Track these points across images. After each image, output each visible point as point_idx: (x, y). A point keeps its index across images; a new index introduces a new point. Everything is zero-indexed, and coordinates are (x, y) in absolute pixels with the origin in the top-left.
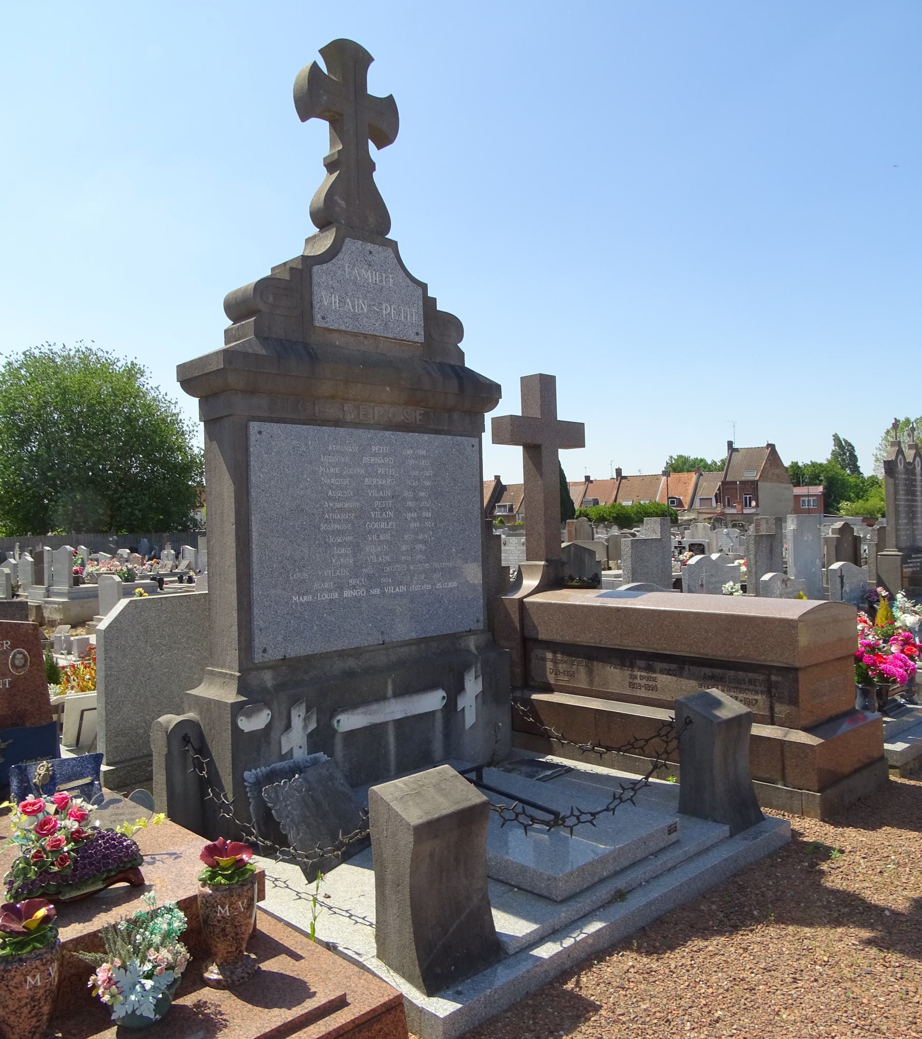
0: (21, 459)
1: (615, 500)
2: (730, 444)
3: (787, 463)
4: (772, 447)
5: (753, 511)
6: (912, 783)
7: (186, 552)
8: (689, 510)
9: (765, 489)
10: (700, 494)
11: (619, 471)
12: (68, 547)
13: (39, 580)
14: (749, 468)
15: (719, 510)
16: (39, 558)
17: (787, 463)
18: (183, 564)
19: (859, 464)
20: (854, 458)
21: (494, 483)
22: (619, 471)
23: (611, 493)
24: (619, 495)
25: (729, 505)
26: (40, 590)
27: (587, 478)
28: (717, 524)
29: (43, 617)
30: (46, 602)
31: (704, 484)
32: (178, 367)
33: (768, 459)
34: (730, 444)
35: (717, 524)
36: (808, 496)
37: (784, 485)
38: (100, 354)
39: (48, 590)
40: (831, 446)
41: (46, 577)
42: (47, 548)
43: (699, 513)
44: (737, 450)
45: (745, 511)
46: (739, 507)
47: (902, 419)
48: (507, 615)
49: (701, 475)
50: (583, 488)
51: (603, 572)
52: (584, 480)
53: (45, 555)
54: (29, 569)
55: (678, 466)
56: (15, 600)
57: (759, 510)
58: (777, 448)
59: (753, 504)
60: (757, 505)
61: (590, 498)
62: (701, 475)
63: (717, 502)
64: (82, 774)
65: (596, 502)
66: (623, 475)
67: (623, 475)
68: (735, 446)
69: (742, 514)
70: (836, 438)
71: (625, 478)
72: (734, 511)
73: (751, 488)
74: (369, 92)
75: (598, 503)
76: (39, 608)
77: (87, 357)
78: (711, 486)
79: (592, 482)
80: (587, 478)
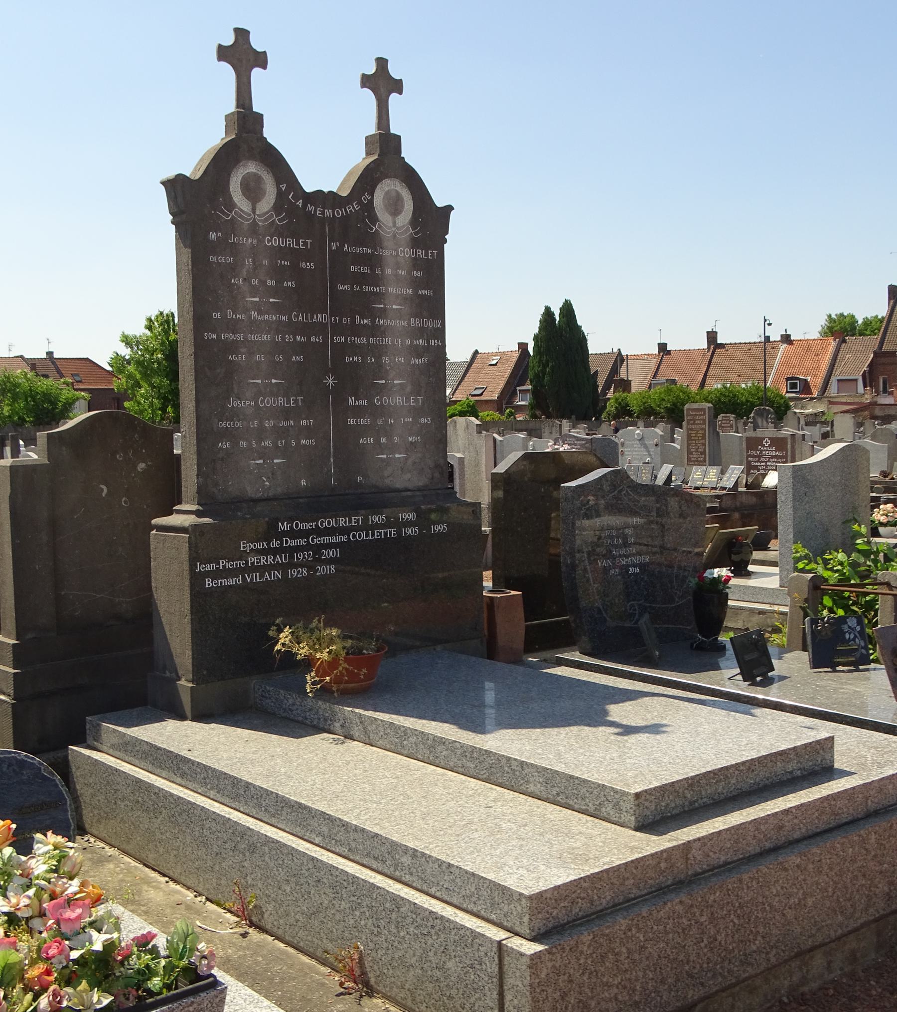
3: (816, 336)
8: (819, 399)
11: (712, 336)
15: (867, 399)
17: (816, 336)
21: (517, 355)
22: (712, 336)
24: (710, 373)
25: (885, 391)
27: (662, 347)
28: (759, 421)
31: (847, 355)
32: (367, 138)
35: (759, 421)
43: (831, 403)
49: (844, 341)
50: (653, 364)
51: (786, 609)
61: (662, 378)
62: (844, 341)
63: (865, 386)
71: (722, 346)
74: (439, 205)
78: (858, 358)
79: (669, 353)
80: (662, 347)
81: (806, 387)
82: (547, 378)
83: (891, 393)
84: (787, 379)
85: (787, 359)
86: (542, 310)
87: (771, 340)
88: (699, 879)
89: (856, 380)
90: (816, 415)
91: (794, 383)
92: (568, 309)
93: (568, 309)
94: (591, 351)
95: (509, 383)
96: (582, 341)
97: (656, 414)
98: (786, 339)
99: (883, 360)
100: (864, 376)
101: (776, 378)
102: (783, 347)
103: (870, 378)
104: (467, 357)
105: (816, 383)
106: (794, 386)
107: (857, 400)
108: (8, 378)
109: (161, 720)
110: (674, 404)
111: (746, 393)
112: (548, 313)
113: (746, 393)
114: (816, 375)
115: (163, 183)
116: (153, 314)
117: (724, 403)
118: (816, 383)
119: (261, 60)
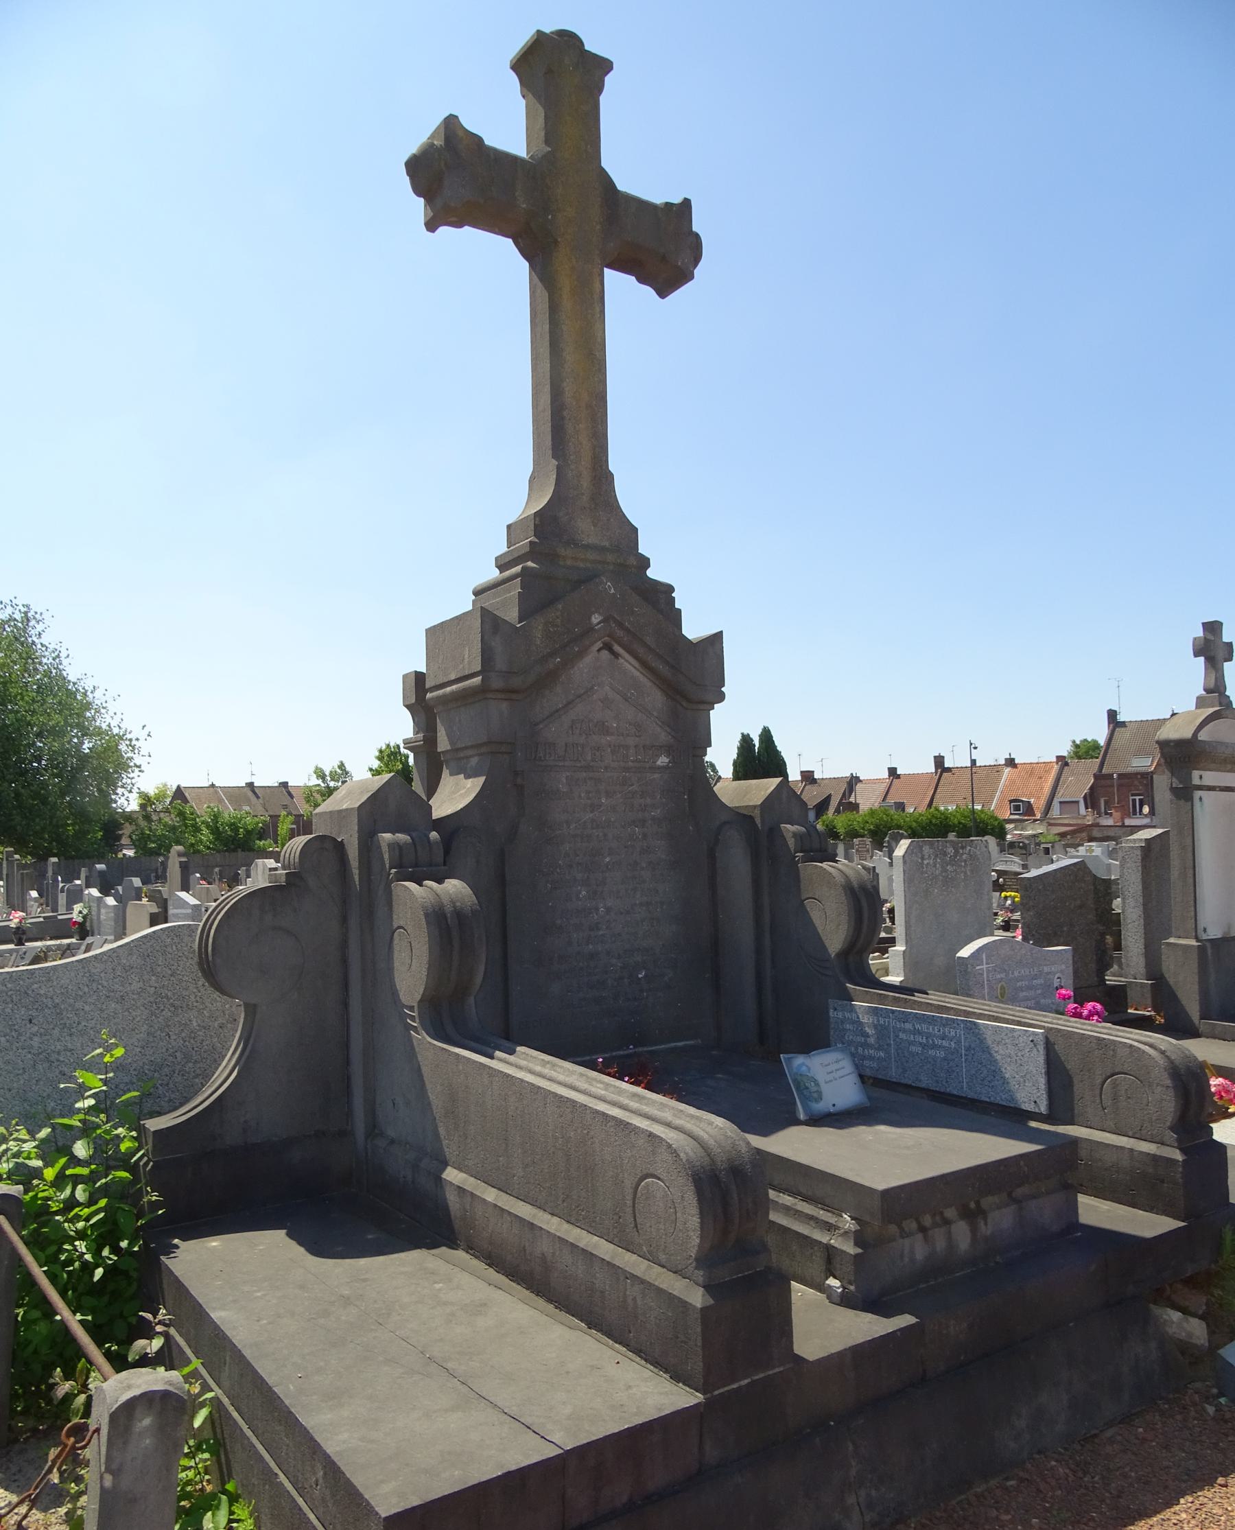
2: (1112, 715)
6: (673, 1045)
11: (939, 761)
14: (1140, 752)
15: (1089, 820)
24: (937, 796)
25: (1106, 813)
27: (893, 772)
34: (1112, 715)
40: (336, 764)
43: (1050, 825)
44: (1123, 724)
46: (1117, 815)
47: (377, 754)
48: (380, 847)
50: (884, 787)
52: (886, 775)
59: (1146, 809)
61: (891, 800)
64: (215, 1060)
65: (901, 806)
68: (1121, 718)
69: (1123, 826)
71: (949, 770)
75: (903, 810)
78: (1079, 783)
79: (898, 777)
80: (893, 772)
81: (1029, 809)
83: (1111, 814)
84: (1011, 801)
85: (1012, 782)
86: (739, 737)
87: (978, 764)
89: (1077, 802)
90: (1034, 836)
91: (1016, 804)
93: (766, 736)
98: (1011, 762)
99: (1103, 782)
100: (1085, 798)
101: (1001, 800)
102: (1007, 770)
103: (1091, 800)
105: (1039, 804)
106: (1017, 808)
107: (1079, 822)
108: (97, 711)
110: (877, 826)
111: (958, 815)
112: (746, 740)
113: (958, 815)
114: (1039, 798)
115: (687, 203)
117: (935, 825)
118: (1039, 804)
119: (662, 247)
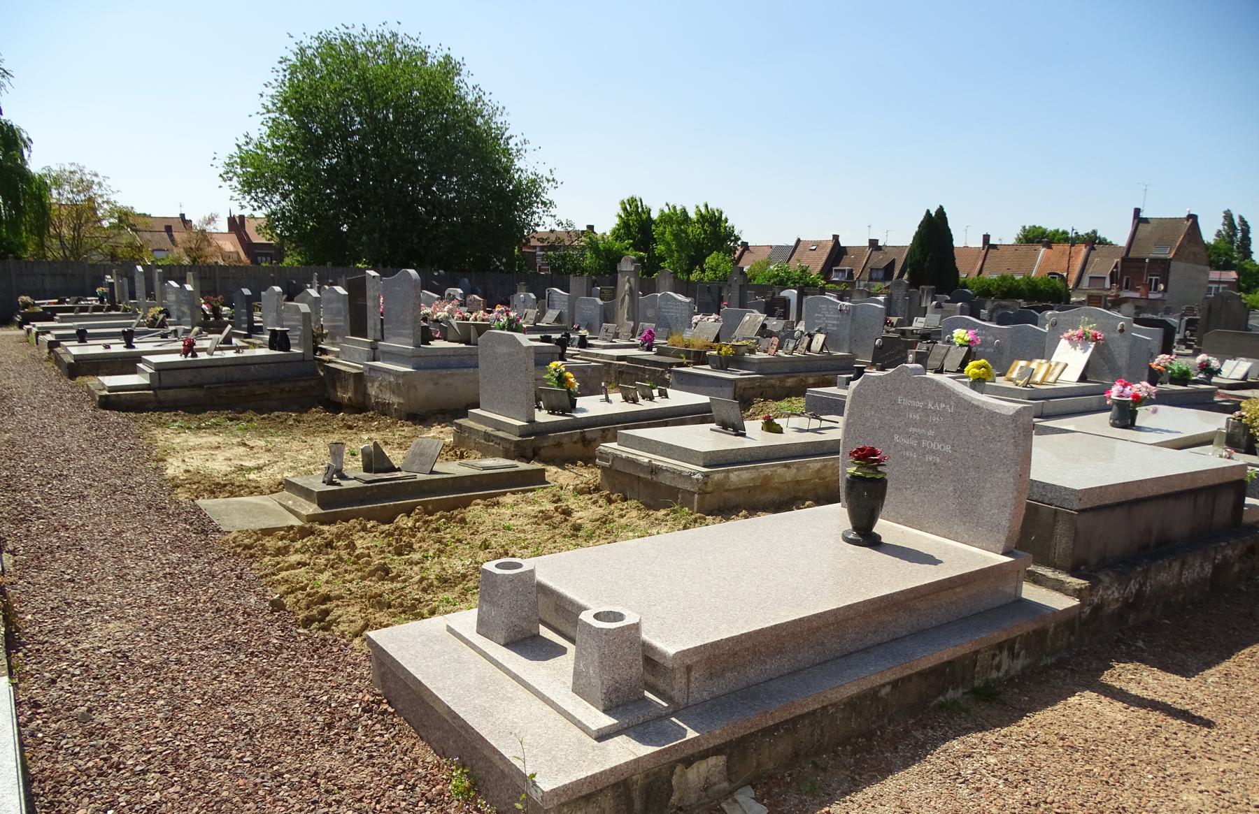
0: (317, 172)
1: (980, 272)
2: (1137, 211)
4: (1193, 218)
5: (1159, 296)
7: (555, 297)
9: (1179, 270)
10: (1091, 271)
11: (986, 238)
12: (412, 272)
13: (358, 327)
14: (1161, 243)
15: (1114, 292)
16: (357, 290)
18: (551, 315)
19: (1252, 248)
20: (1246, 240)
21: (831, 244)
22: (986, 238)
23: (974, 266)
25: (1127, 288)
26: (360, 345)
29: (366, 395)
30: (372, 368)
31: (1096, 259)
33: (1187, 234)
36: (1220, 282)
37: (1201, 267)
38: (407, 42)
39: (374, 347)
41: (370, 323)
42: (373, 273)
44: (1146, 221)
45: (1151, 296)
49: (1093, 249)
53: (369, 285)
54: (343, 307)
55: (1035, 238)
56: (335, 438)
57: (1167, 296)
58: (1200, 221)
60: (1165, 290)
62: (1093, 249)
63: (1112, 282)
66: (991, 242)
67: (991, 242)
68: (1143, 215)
70: (1228, 216)
71: (994, 247)
72: (1137, 295)
73: (1162, 267)
76: (359, 377)
77: (391, 45)
78: (1104, 266)
79: (879, 248)
82: (926, 264)
88: (520, 452)
92: (941, 211)
93: (941, 211)
94: (956, 243)
95: (826, 264)
96: (949, 237)
97: (578, 270)
100: (1112, 274)
104: (793, 243)
109: (1064, 696)
116: (626, 198)
